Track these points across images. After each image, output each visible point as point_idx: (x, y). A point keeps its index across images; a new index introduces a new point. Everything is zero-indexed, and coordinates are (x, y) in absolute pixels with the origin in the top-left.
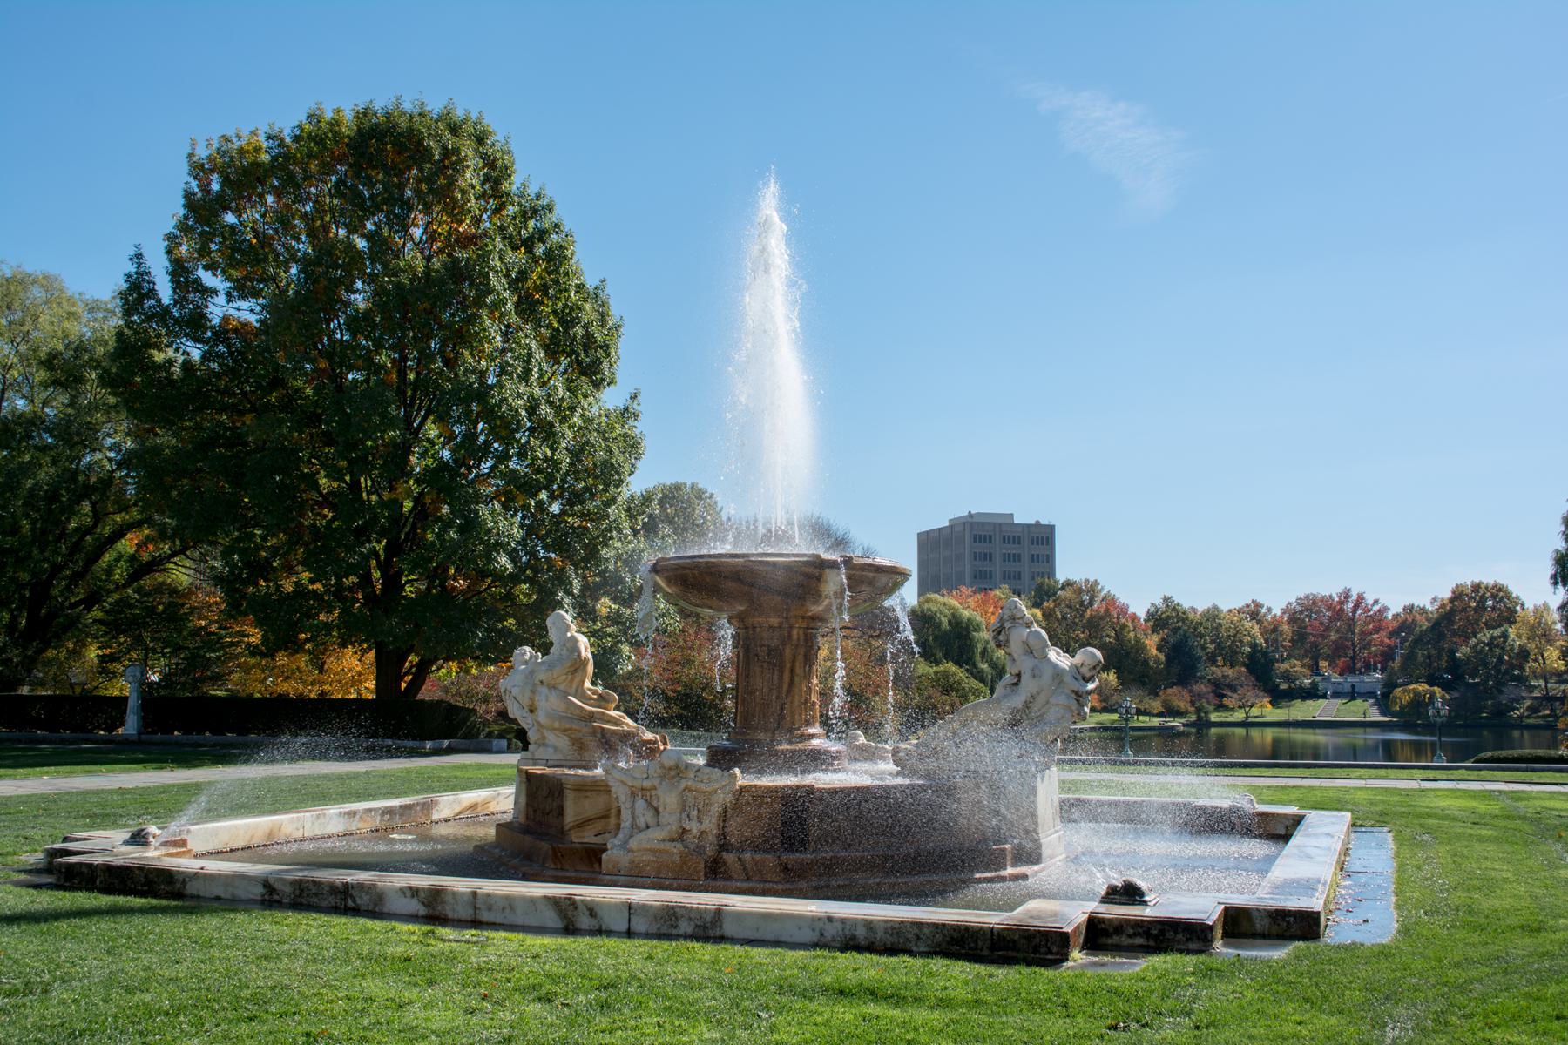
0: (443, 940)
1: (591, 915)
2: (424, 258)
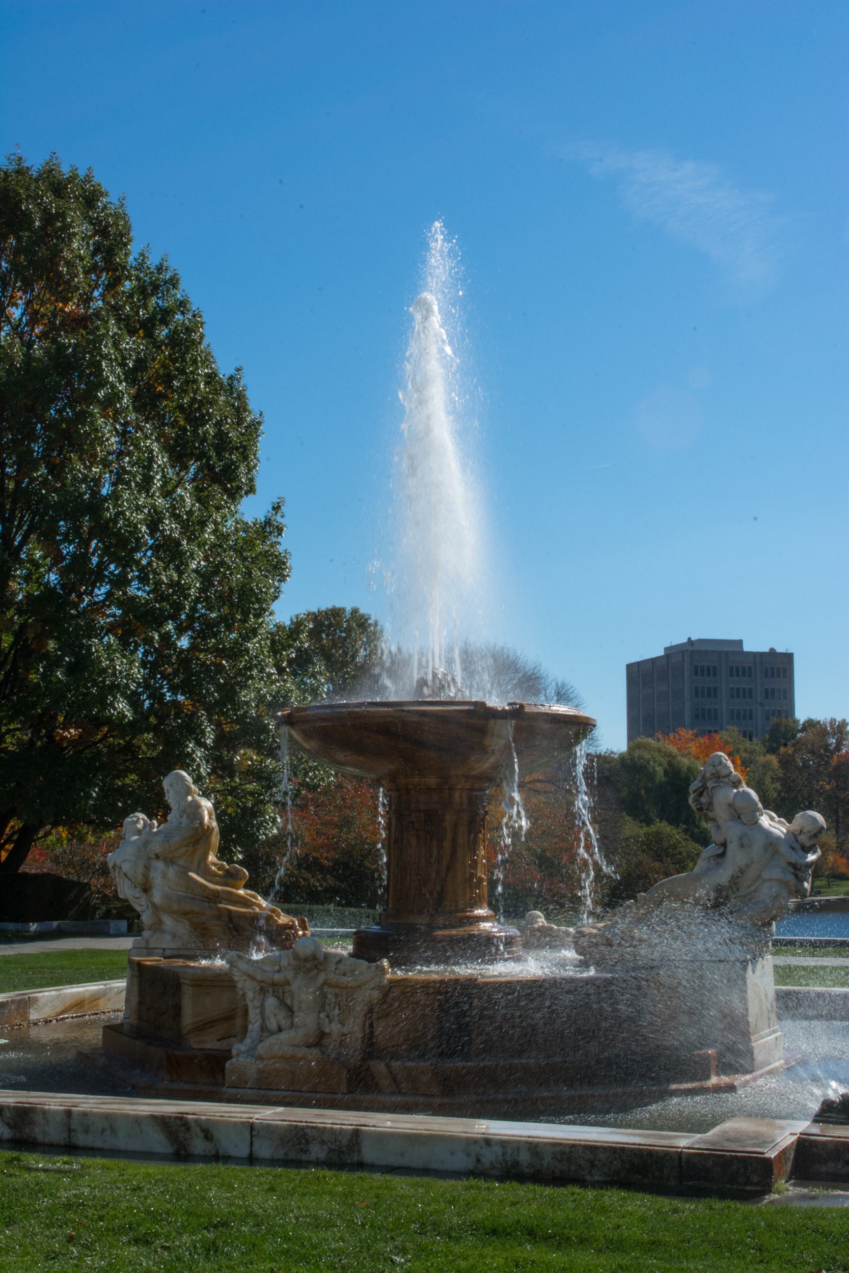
0: (29, 1169)
2: (23, 345)
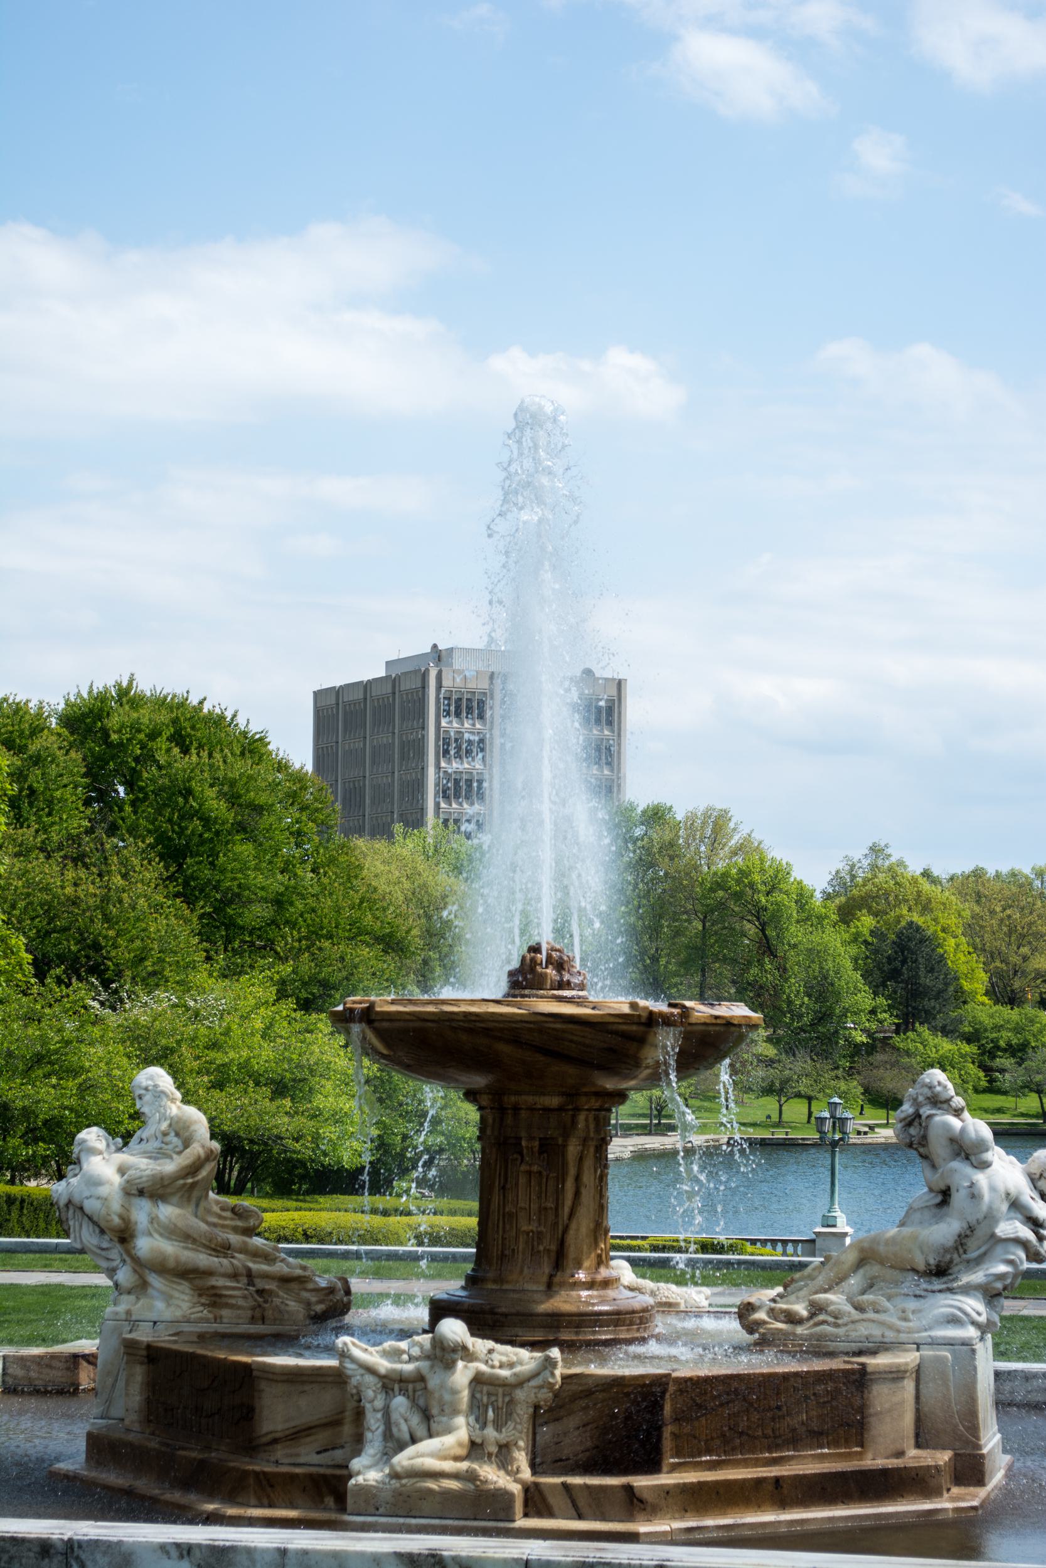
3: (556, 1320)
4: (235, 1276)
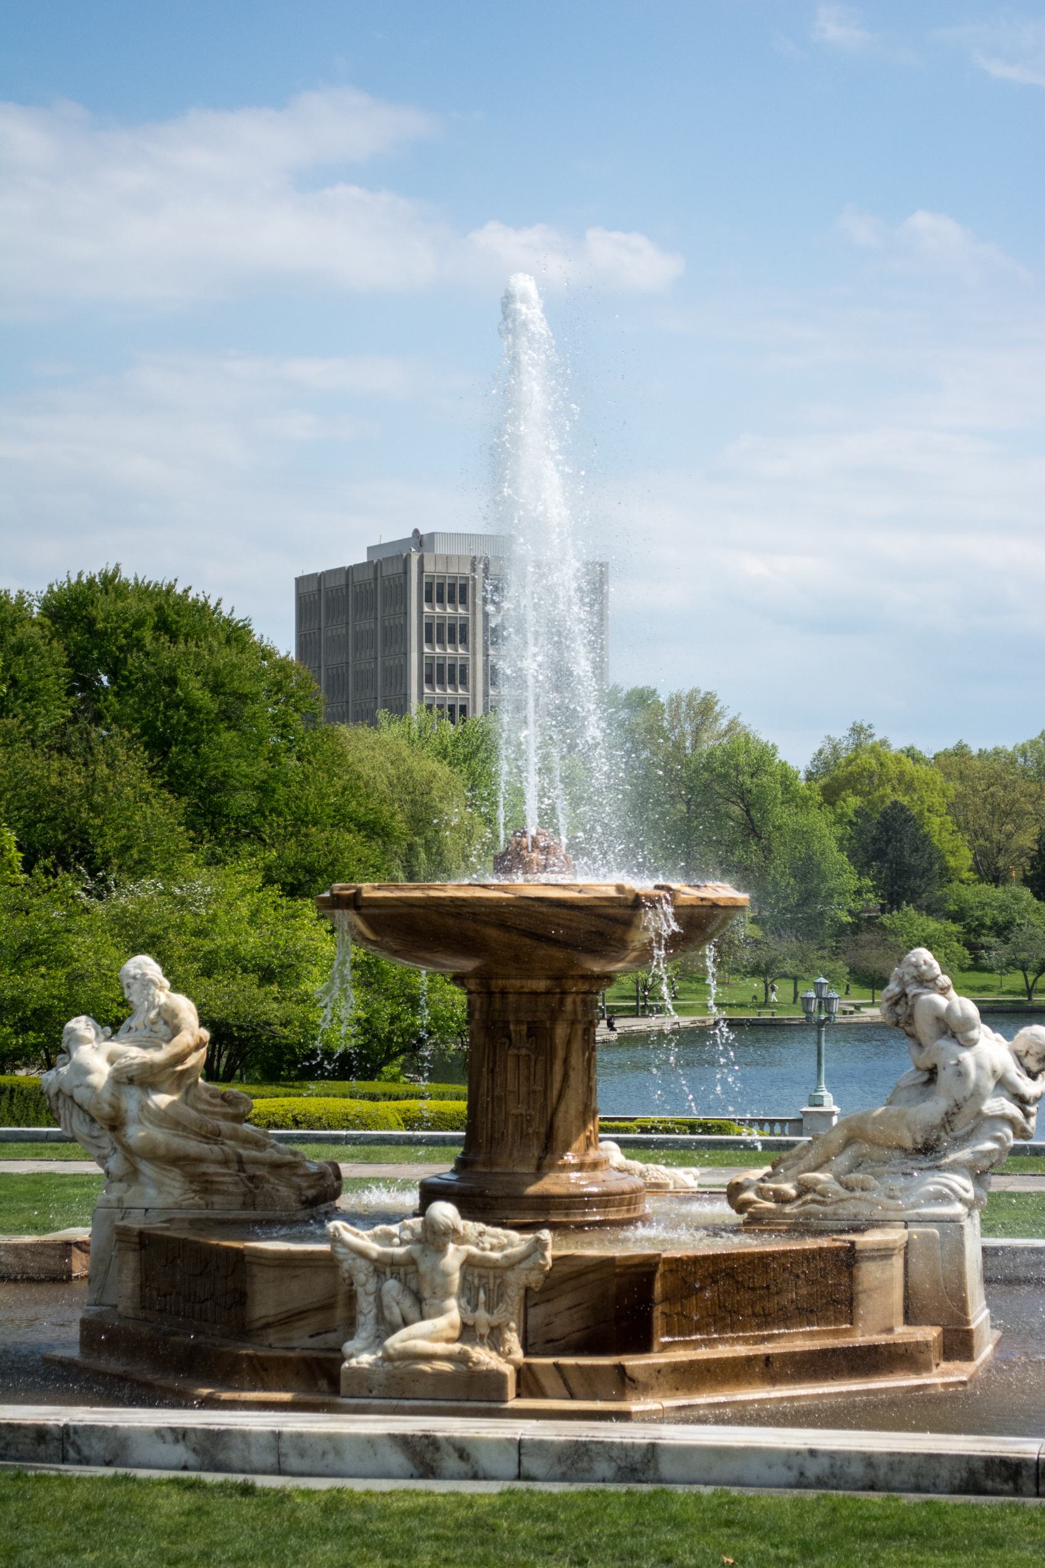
1: (461, 1457)
3: (546, 1202)
4: (225, 1162)
